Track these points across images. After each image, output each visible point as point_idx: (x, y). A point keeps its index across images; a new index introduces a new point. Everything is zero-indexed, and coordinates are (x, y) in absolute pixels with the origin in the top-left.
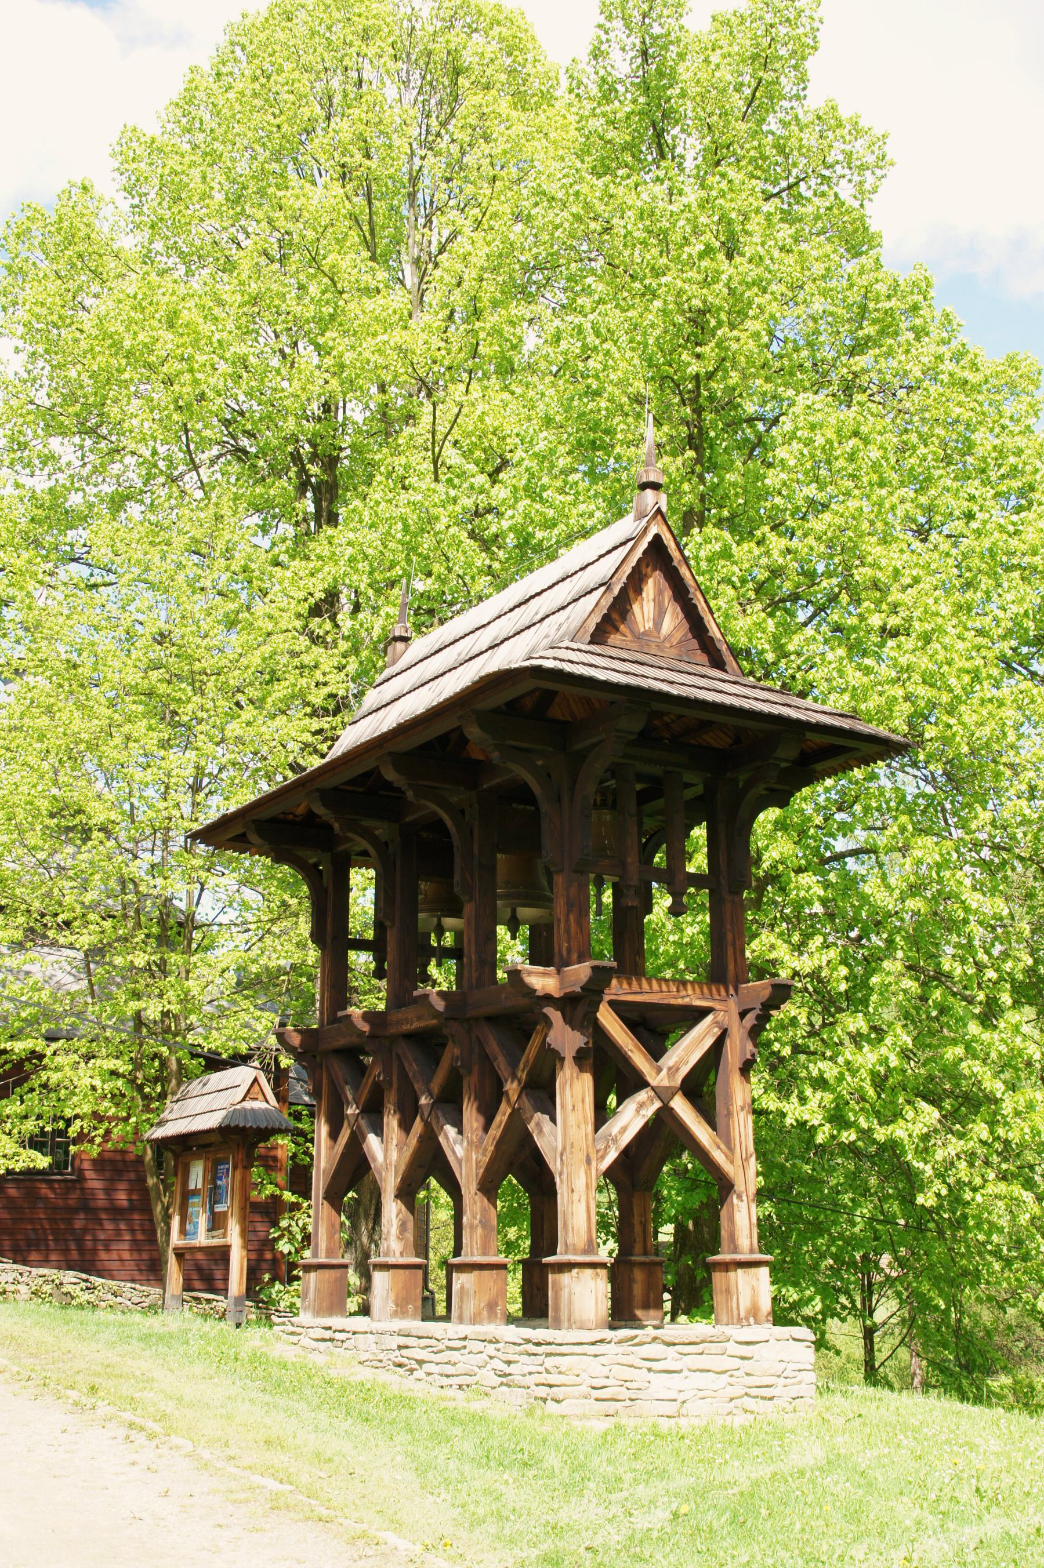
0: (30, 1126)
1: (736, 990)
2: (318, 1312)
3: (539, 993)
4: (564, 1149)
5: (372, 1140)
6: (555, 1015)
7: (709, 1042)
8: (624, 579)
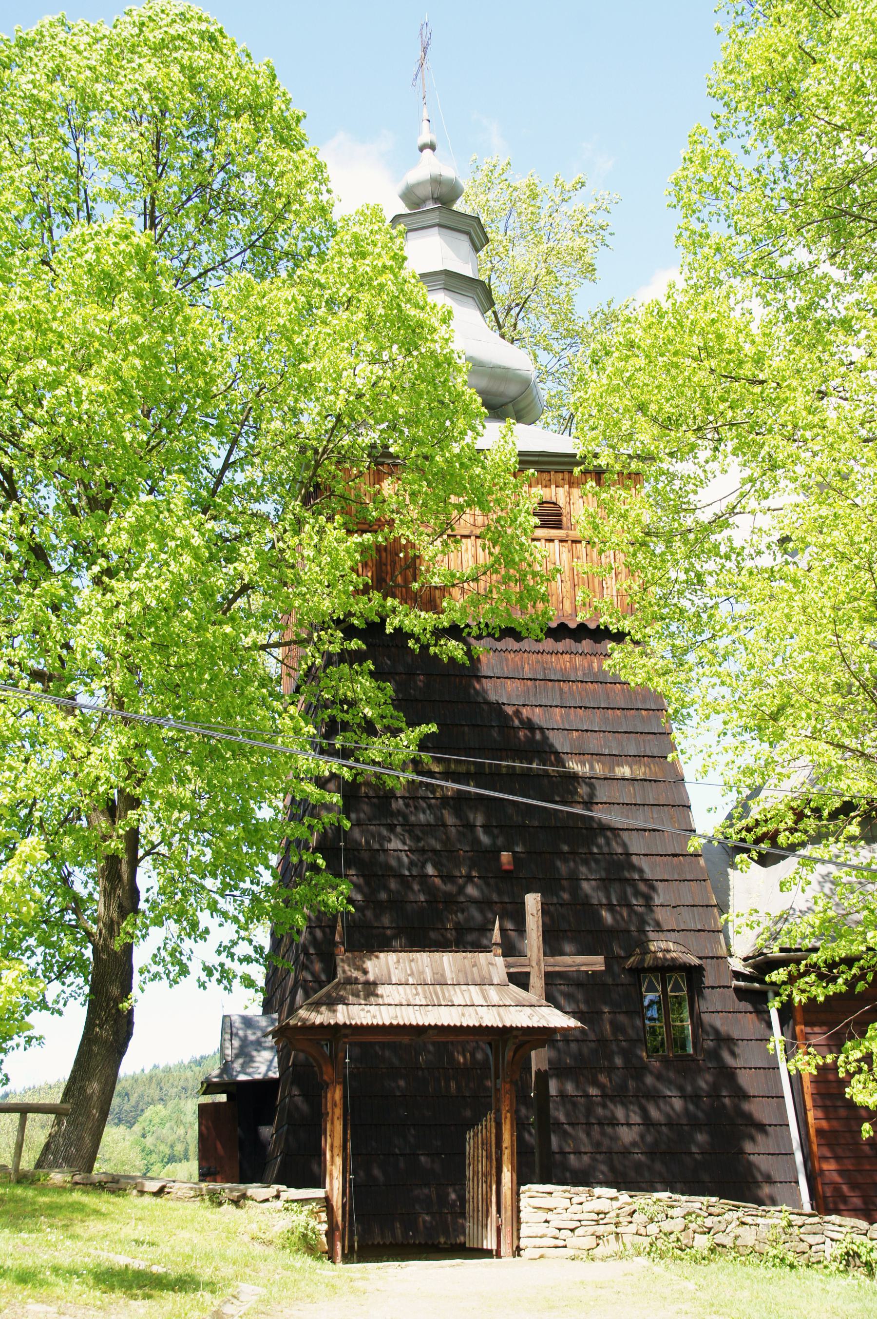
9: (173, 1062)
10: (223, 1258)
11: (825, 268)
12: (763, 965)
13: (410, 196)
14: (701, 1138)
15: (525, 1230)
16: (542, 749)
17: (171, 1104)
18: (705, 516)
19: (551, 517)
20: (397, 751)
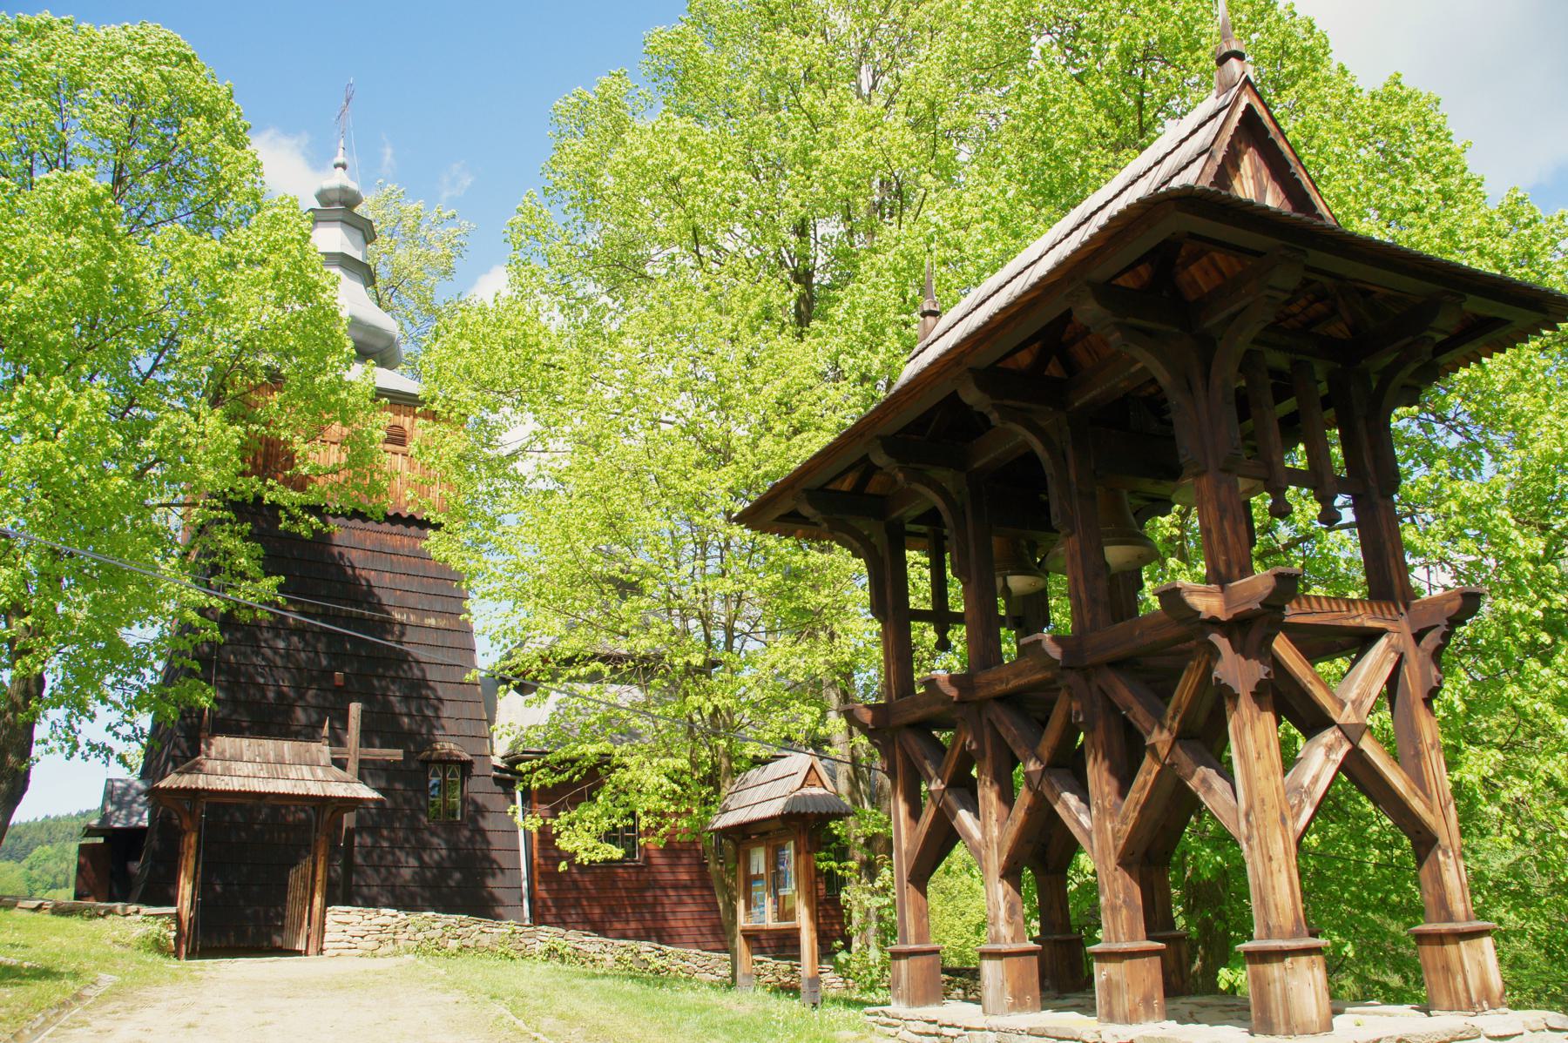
0: (605, 824)
1: (1407, 607)
2: (913, 1001)
3: (1204, 616)
4: (1250, 807)
5: (965, 816)
6: (1222, 643)
7: (1387, 670)
8: (1225, 147)
9: (62, 813)
10: (87, 955)
11: (605, 299)
12: (513, 760)
13: (322, 196)
14: (457, 876)
15: (327, 937)
16: (379, 606)
17: (57, 845)
18: (505, 452)
19: (397, 438)
20: (260, 591)
